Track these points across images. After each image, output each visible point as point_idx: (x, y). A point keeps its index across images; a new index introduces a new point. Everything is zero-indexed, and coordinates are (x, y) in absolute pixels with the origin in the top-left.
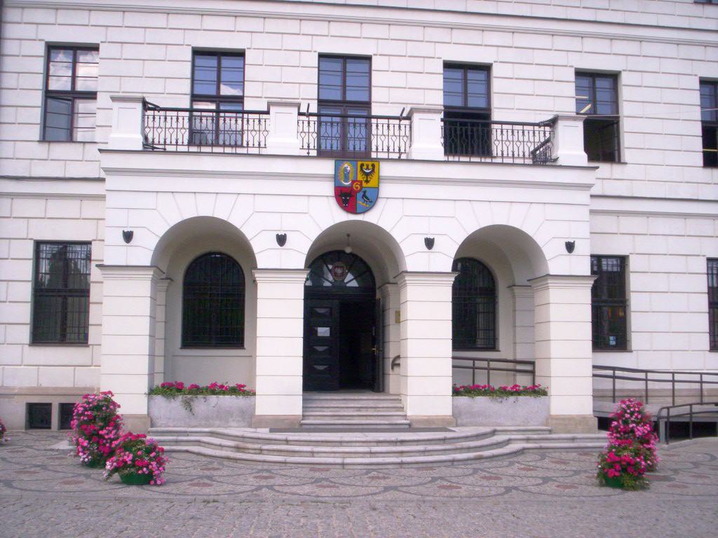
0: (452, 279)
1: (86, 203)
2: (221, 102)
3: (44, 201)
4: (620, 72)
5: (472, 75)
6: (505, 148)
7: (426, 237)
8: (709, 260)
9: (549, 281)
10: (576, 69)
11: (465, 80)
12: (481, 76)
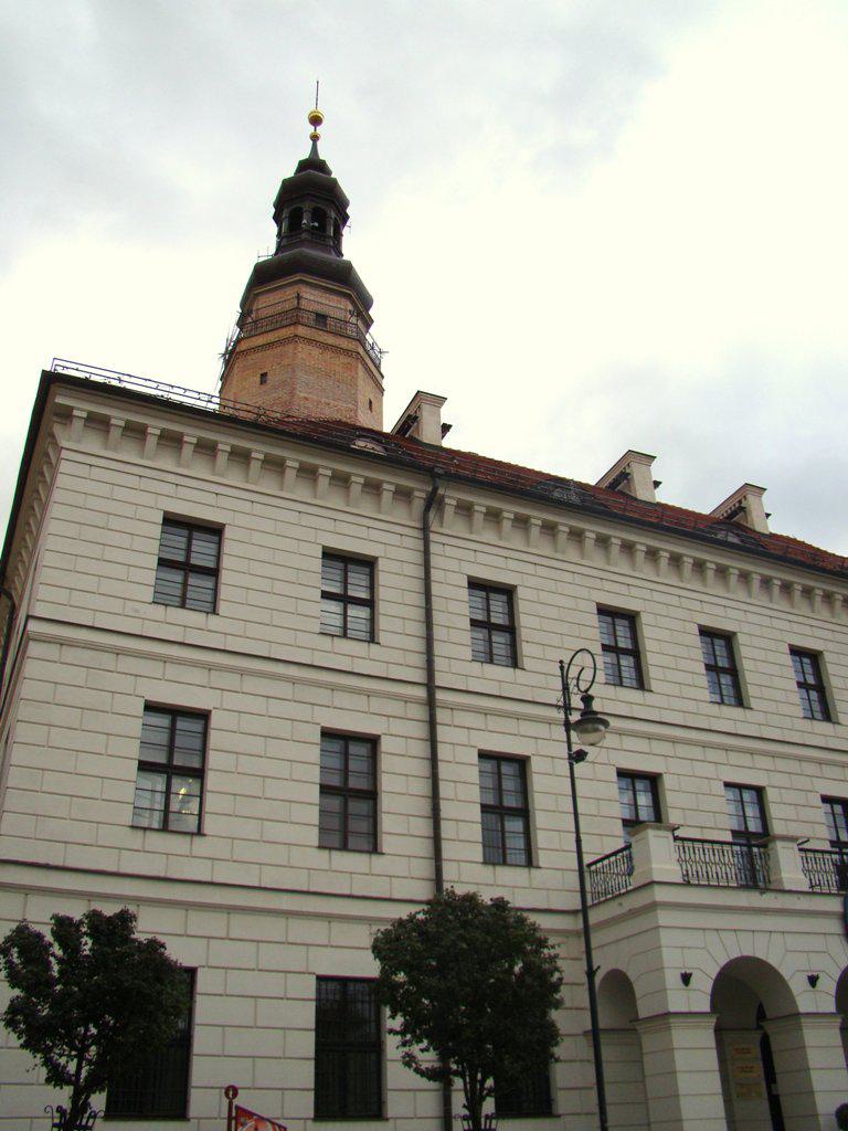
0: (713, 1021)
1: (336, 926)
2: (351, 796)
3: (184, 912)
4: (379, 736)
5: (182, 724)
6: (699, 870)
7: (683, 972)
8: (320, 979)
9: (671, 1020)
10: (322, 727)
11: (173, 729)
12: (197, 726)
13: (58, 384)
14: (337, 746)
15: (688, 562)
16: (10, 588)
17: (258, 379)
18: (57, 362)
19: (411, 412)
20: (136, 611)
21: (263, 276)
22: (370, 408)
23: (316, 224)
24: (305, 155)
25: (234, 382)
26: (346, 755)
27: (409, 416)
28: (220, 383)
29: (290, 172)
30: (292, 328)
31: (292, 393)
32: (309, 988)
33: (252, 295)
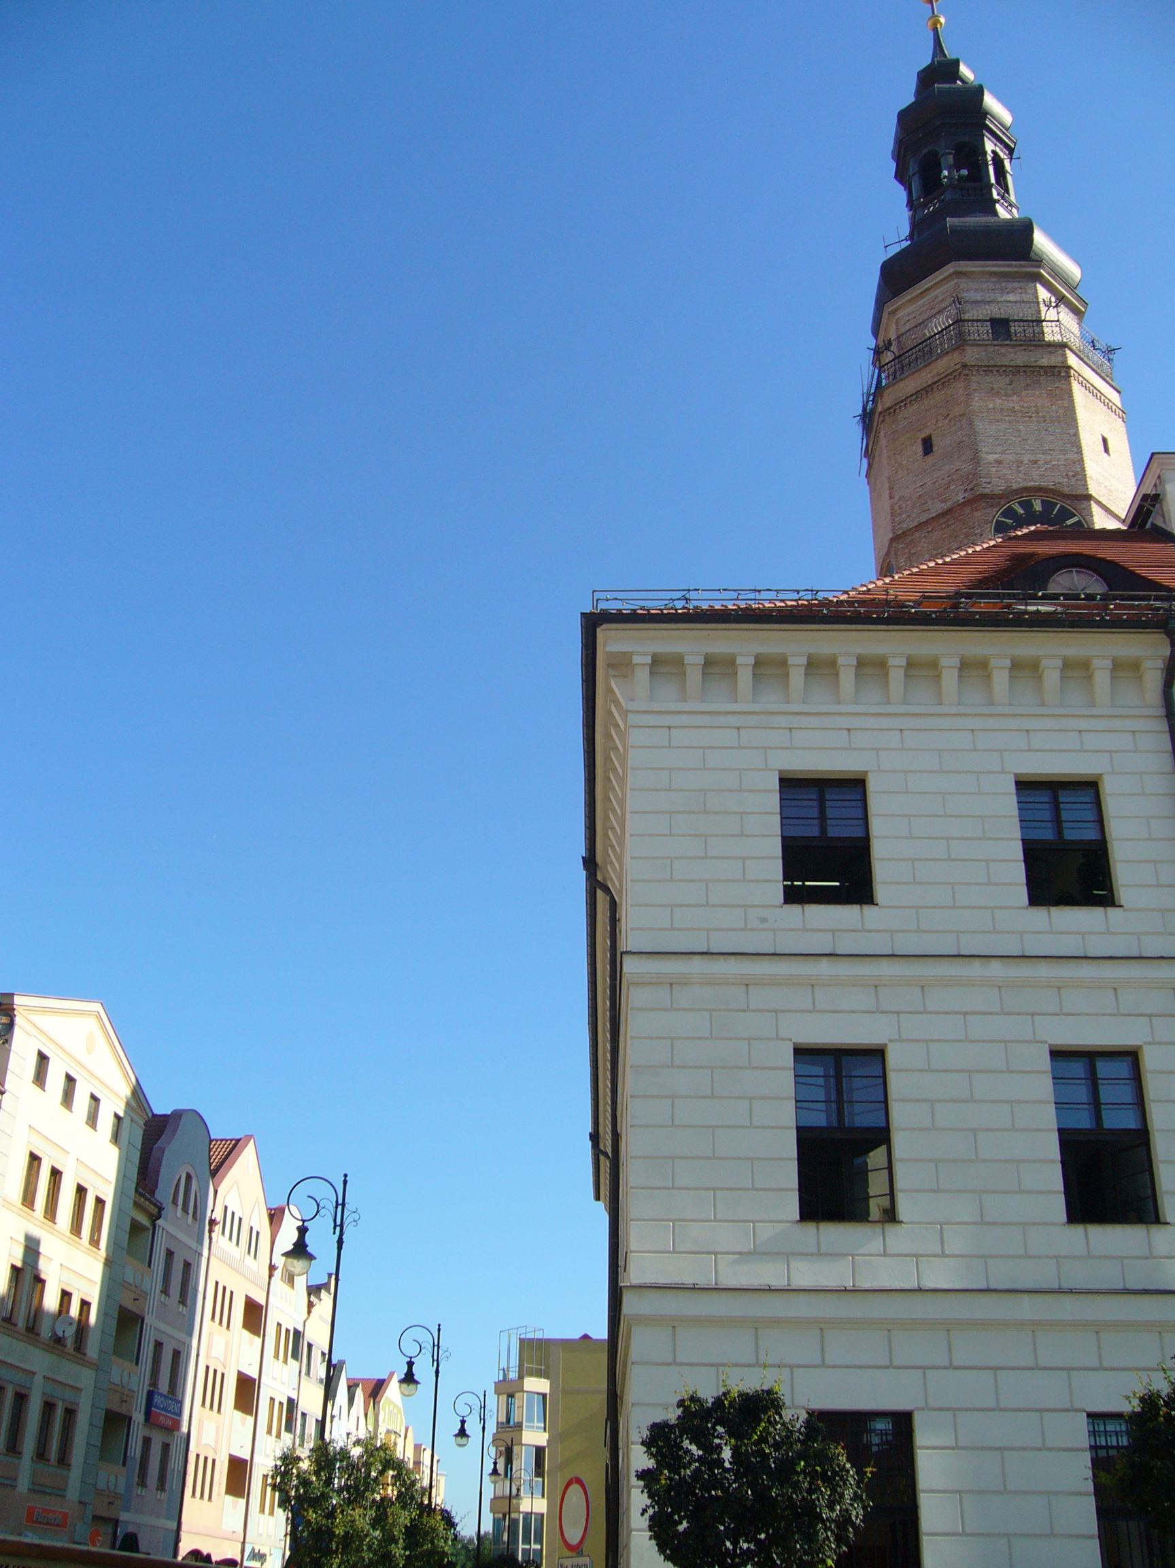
5: (1103, 1068)
8: (1092, 1416)
13: (605, 626)
14: (1077, 1068)
15: (847, 663)
16: (605, 879)
17: (919, 448)
18: (597, 596)
19: (1148, 489)
20: (763, 920)
21: (898, 277)
22: (1106, 450)
23: (964, 172)
24: (925, 60)
25: (885, 462)
26: (1093, 1081)
27: (1145, 497)
28: (865, 461)
29: (906, 96)
30: (956, 354)
31: (976, 460)
32: (1078, 1433)
33: (885, 316)
